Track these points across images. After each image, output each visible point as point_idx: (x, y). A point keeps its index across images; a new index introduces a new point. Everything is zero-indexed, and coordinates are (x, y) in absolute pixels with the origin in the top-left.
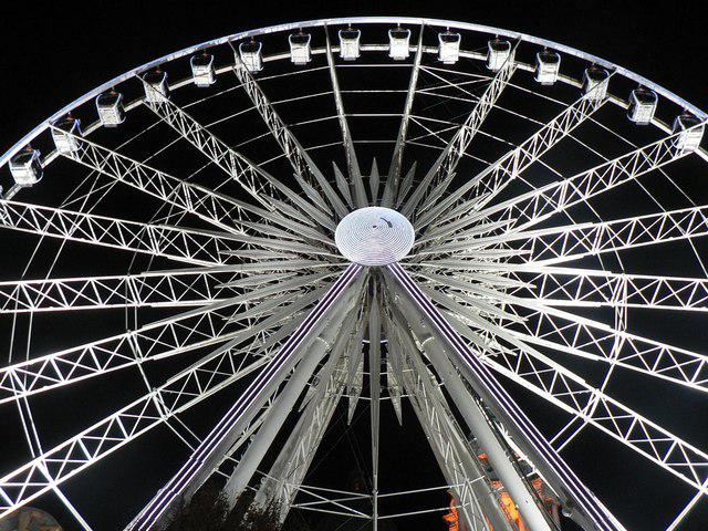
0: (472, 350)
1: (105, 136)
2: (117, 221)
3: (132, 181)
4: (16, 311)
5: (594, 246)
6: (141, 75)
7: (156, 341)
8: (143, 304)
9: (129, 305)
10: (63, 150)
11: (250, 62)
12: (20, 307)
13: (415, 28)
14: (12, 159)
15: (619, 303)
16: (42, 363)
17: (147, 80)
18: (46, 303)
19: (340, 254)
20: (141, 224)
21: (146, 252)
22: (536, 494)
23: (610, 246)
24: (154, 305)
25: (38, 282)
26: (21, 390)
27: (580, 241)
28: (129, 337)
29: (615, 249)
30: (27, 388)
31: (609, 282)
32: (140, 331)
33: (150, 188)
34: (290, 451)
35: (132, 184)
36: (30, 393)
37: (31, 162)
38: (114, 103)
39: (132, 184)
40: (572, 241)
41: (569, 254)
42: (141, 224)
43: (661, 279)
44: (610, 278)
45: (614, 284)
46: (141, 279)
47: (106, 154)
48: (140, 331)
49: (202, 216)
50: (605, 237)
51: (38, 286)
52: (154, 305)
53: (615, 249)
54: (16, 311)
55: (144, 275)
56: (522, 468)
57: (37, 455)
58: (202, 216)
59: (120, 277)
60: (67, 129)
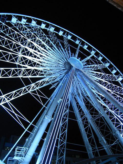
0: (71, 83)
4: (65, 149)
5: (24, 70)
13: (81, 40)
15: (20, 55)
19: (84, 113)
21: (94, 138)
22: (39, 126)
23: (19, 70)
26: (95, 149)
27: (26, 73)
28: (16, 153)
29: (18, 68)
30: (95, 147)
31: (21, 62)
34: (82, 132)
36: (96, 147)
40: (29, 73)
41: (31, 76)
43: (10, 77)
44: (20, 64)
45: (20, 62)
50: (20, 72)
53: (18, 68)
56: (64, 81)
57: (103, 148)
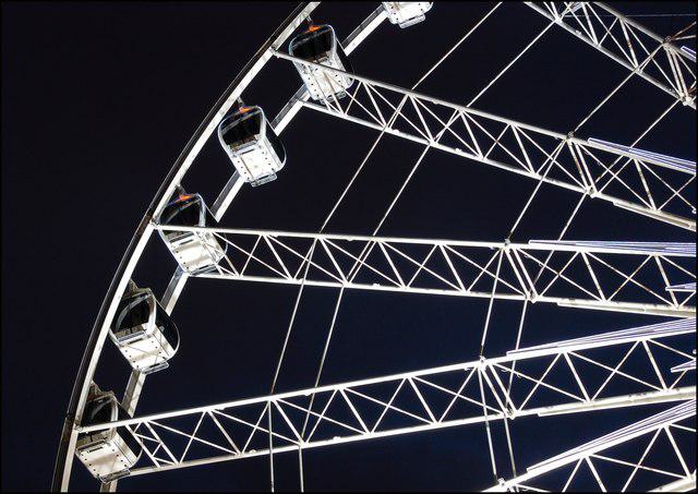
1: (257, 204)
2: (442, 244)
3: (576, 27)
4: (493, 296)
6: (284, 49)
7: (638, 466)
8: (518, 413)
9: (493, 417)
10: (193, 268)
11: (324, 82)
12: (502, 289)
14: (113, 327)
16: (525, 408)
17: (299, 54)
18: (326, 431)
20: (491, 245)
24: (541, 412)
25: (307, 392)
32: (524, 478)
33: (497, 155)
35: (458, 152)
37: (153, 317)
38: (329, 48)
39: (458, 152)
42: (491, 245)
46: (509, 364)
47: (396, 98)
48: (524, 478)
49: (617, 202)
51: (303, 401)
52: (541, 412)
54: (493, 296)
55: (514, 356)
58: (617, 202)
59: (465, 366)
60: (194, 222)
